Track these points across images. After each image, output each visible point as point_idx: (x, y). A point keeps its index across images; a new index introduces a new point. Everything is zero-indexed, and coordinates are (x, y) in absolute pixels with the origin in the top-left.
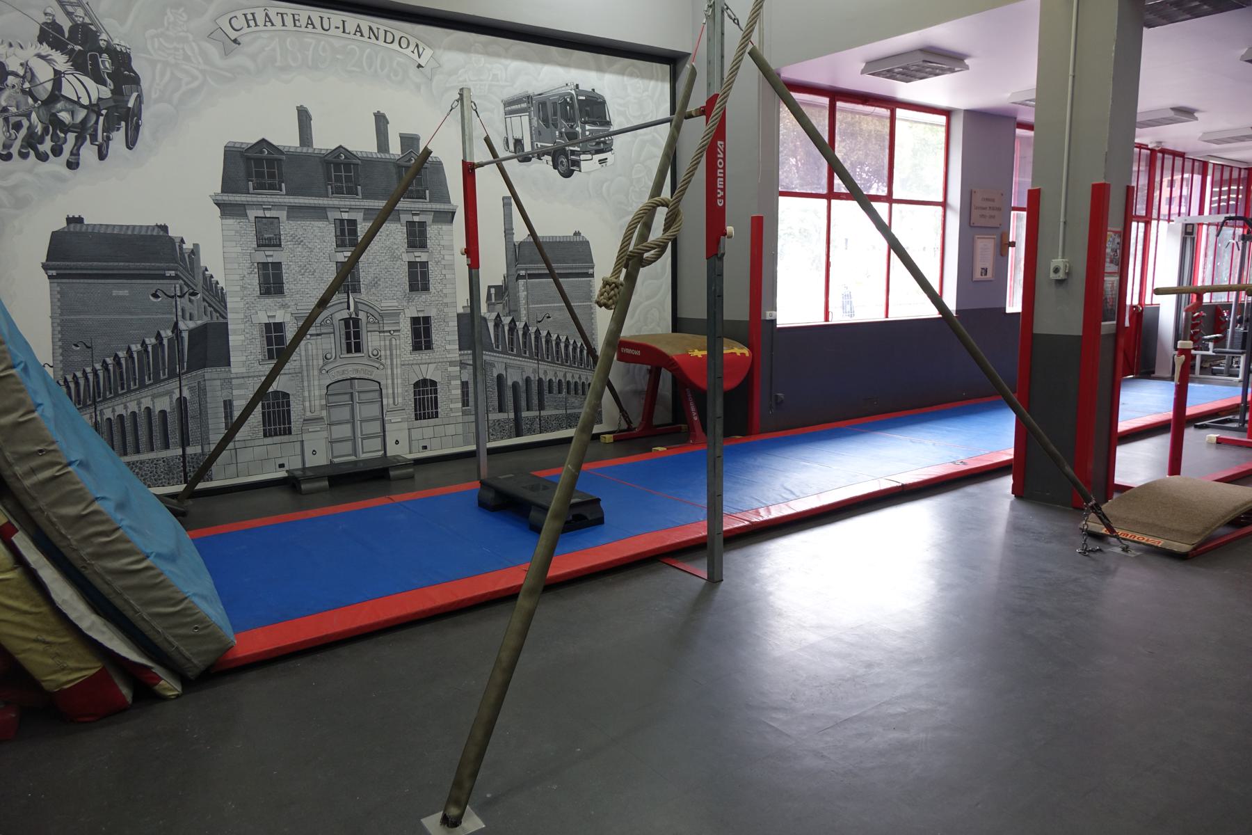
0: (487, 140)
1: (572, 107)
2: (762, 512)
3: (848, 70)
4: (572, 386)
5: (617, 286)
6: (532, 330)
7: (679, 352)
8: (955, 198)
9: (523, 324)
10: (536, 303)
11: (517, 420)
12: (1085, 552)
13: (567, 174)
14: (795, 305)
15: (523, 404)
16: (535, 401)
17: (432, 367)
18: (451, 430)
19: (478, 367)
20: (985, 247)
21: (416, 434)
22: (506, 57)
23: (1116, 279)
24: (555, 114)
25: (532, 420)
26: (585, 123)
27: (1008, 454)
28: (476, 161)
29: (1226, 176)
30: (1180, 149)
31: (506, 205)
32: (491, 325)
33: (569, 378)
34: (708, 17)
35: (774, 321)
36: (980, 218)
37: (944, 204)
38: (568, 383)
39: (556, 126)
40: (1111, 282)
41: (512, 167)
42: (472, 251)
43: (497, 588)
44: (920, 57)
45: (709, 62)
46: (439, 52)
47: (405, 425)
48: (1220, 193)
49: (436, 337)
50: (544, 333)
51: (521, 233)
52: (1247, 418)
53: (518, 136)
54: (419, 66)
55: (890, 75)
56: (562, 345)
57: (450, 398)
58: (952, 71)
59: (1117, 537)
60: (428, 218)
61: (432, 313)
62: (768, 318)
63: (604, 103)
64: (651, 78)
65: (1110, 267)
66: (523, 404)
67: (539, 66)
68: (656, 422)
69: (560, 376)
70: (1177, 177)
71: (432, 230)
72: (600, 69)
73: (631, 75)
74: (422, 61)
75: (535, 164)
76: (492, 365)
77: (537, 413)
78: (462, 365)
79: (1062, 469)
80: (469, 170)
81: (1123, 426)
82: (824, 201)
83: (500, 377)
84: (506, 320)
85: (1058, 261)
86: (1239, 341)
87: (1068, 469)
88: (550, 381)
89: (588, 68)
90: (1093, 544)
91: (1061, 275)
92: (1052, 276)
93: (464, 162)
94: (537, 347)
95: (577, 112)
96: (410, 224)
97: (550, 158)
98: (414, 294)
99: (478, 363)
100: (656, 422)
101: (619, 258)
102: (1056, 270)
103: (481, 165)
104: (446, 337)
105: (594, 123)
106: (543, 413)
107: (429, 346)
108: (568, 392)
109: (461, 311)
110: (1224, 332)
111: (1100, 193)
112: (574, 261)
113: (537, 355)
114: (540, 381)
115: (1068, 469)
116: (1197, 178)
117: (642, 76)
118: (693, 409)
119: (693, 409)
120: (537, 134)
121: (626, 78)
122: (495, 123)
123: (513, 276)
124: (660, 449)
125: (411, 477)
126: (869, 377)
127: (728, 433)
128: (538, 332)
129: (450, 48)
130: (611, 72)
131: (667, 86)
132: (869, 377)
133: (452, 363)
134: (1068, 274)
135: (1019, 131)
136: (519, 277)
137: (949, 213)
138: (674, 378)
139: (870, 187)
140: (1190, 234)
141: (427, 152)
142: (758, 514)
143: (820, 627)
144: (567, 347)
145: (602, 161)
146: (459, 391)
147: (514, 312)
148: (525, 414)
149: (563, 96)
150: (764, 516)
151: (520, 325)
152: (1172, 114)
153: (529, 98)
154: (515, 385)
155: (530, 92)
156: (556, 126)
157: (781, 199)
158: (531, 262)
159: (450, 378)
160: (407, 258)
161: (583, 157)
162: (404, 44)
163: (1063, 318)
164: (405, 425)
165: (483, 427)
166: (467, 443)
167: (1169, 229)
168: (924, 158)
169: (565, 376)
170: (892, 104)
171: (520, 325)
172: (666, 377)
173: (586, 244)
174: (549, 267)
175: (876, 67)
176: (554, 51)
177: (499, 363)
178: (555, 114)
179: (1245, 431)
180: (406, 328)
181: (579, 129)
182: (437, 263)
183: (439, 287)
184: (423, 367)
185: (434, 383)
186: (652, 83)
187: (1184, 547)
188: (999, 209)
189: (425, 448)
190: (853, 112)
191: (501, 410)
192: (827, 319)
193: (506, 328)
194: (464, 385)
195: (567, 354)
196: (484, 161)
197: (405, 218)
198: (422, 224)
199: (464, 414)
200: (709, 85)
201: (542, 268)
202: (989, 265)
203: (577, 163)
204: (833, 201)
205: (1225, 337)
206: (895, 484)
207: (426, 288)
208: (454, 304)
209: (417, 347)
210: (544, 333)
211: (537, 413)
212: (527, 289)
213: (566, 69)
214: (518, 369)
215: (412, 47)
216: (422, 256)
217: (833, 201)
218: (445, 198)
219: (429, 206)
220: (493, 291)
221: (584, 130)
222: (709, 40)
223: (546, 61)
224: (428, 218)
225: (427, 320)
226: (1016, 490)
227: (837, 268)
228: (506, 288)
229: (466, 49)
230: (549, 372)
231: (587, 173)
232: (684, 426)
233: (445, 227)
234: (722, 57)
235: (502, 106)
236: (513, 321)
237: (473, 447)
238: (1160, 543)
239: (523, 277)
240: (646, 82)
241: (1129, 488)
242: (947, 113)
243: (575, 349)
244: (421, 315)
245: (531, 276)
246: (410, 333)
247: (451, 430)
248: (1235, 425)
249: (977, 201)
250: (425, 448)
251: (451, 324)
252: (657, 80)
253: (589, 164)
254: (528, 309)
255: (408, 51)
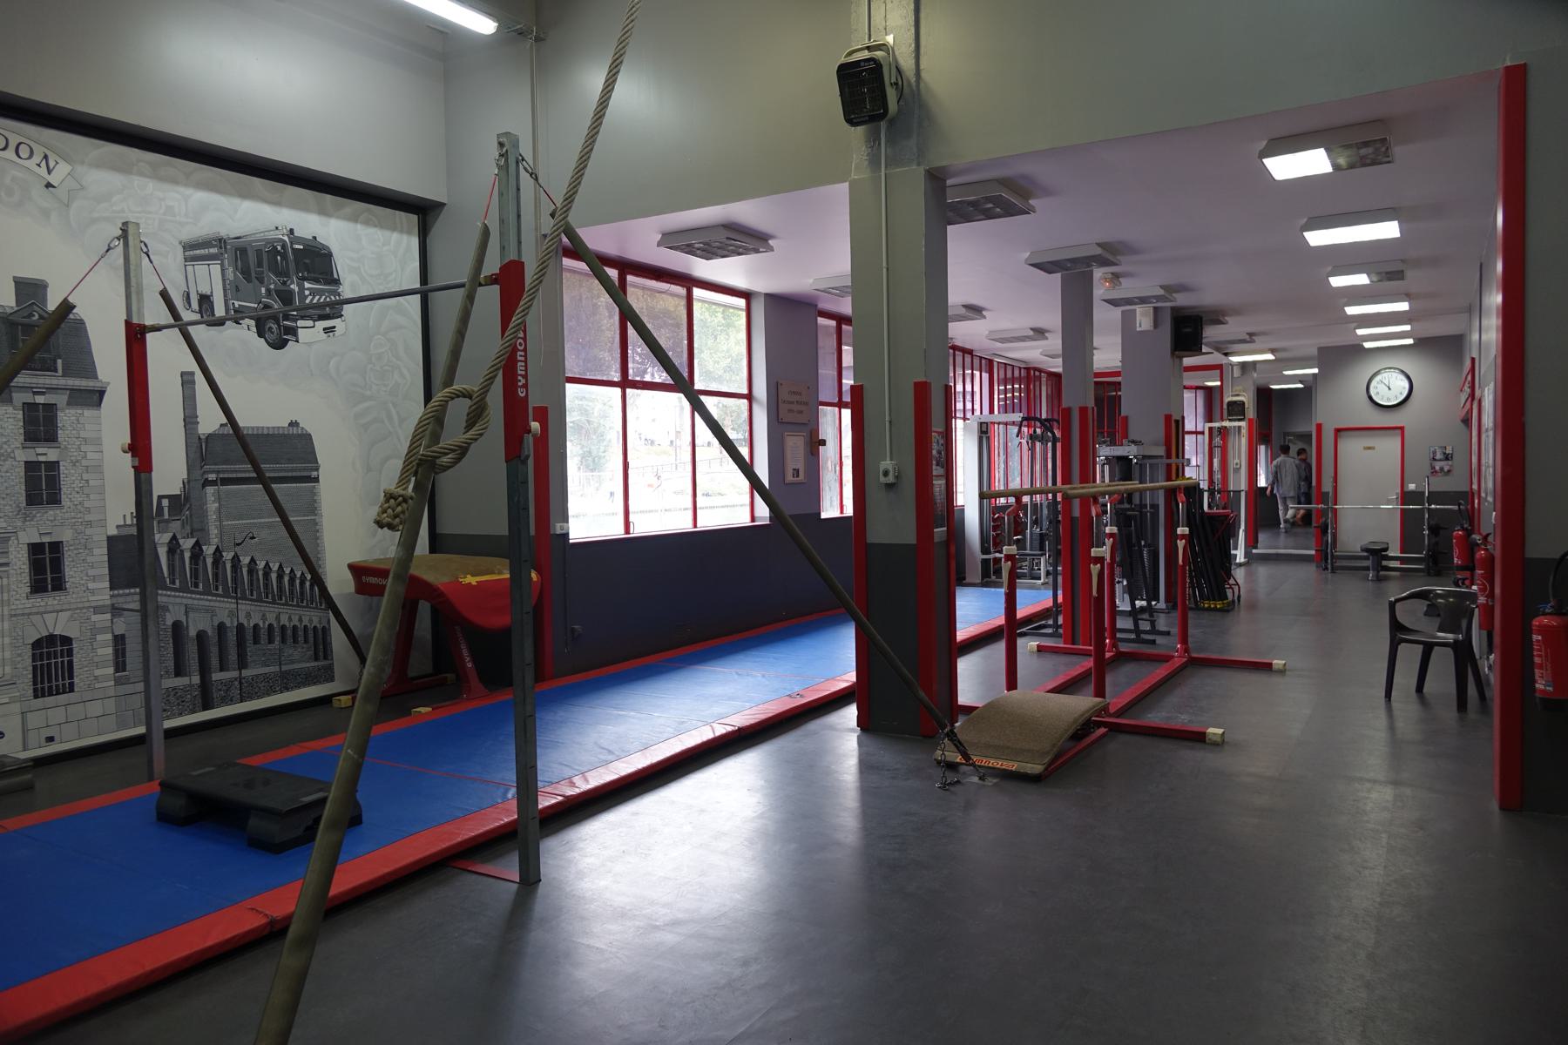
0: (164, 295)
1: (284, 256)
2: (577, 780)
3: (641, 239)
4: (289, 632)
5: (405, 500)
6: (228, 556)
7: (445, 579)
8: (761, 390)
9: (212, 549)
10: (235, 520)
11: (205, 686)
12: (945, 786)
13: (279, 345)
14: (590, 515)
15: (215, 661)
16: (233, 656)
17: (64, 616)
18: (95, 709)
19: (148, 612)
20: (795, 444)
21: (34, 720)
22: (186, 185)
23: (943, 482)
24: (260, 264)
25: (228, 684)
26: (304, 279)
27: (848, 676)
28: (148, 322)
29: (1009, 375)
30: (968, 346)
31: (187, 380)
32: (162, 552)
33: (284, 620)
34: (500, 167)
35: (566, 535)
36: (792, 414)
37: (749, 397)
38: (283, 628)
39: (261, 281)
40: (939, 484)
41: (199, 333)
42: (140, 446)
43: (210, 943)
44: (722, 235)
45: (502, 221)
46: (80, 169)
47: (16, 707)
48: (1006, 391)
49: (71, 571)
50: (245, 560)
51: (210, 420)
52: (1060, 621)
53: (205, 290)
54: (49, 185)
55: (690, 250)
56: (274, 576)
57: (94, 662)
58: (757, 251)
59: (973, 764)
60: (60, 399)
61: (66, 536)
62: (559, 532)
63: (330, 255)
64: (393, 229)
65: (937, 470)
66: (215, 661)
67: (236, 201)
68: (411, 673)
69: (271, 619)
70: (977, 373)
71: (67, 418)
72: (323, 212)
73: (367, 223)
74: (53, 179)
75: (230, 329)
76: (166, 609)
77: (235, 674)
78: (116, 611)
79: (904, 696)
80: (136, 336)
81: (961, 635)
82: (618, 391)
83: (177, 626)
84: (187, 544)
85: (887, 464)
86: (1037, 543)
87: (922, 694)
88: (256, 626)
89: (306, 209)
90: (951, 777)
91: (891, 479)
92: (882, 479)
93: (128, 323)
94: (235, 580)
95: (292, 266)
96: (29, 408)
97: (253, 323)
98: (34, 510)
99: (150, 607)
100: (411, 673)
101: (407, 463)
102: (886, 474)
103: (157, 329)
104: (88, 574)
105: (316, 281)
106: (245, 673)
107: (59, 585)
108: (283, 640)
109: (113, 531)
110: (1023, 532)
111: (922, 390)
112: (290, 461)
113: (235, 591)
114: (240, 627)
115: (922, 694)
116: (986, 376)
117: (381, 225)
118: (465, 653)
119: (465, 653)
120: (232, 290)
121: (359, 226)
122: (168, 269)
123: (197, 481)
124: (423, 710)
125: (29, 787)
126: (683, 601)
127: (539, 677)
128: (236, 560)
129: (100, 165)
130: (338, 217)
131: (415, 241)
132: (683, 601)
133: (98, 610)
134: (897, 477)
135: (821, 320)
136: (207, 483)
137: (755, 407)
138: (435, 612)
139: (645, 372)
140: (984, 431)
141: (66, 307)
142: (573, 784)
143: (676, 923)
144: (280, 577)
145: (328, 330)
146: (110, 650)
147: (199, 532)
148: (217, 676)
149: (271, 242)
150: (582, 786)
151: (209, 550)
152: (963, 311)
153: (221, 242)
154: (201, 636)
155: (224, 233)
156: (261, 281)
157: (568, 385)
158: (226, 462)
159: (95, 631)
160: (23, 456)
161: (300, 323)
162: (24, 152)
163: (895, 527)
164: (16, 707)
165: (156, 703)
166: (122, 725)
167: (965, 428)
168: (725, 349)
169: (278, 618)
170: (689, 282)
171: (209, 550)
172: (424, 609)
173: (307, 438)
174: (257, 468)
175: (672, 239)
176: (257, 182)
177: (174, 605)
178: (260, 264)
179: (1060, 636)
180: (19, 559)
181: (294, 287)
182: (74, 464)
183: (78, 498)
184: (49, 618)
185: (67, 640)
186: (395, 236)
187: (1035, 768)
188: (806, 404)
189: (50, 739)
190: (644, 288)
191: (179, 672)
192: (627, 531)
193: (187, 555)
194: (119, 641)
195: (302, 593)
196: (163, 322)
197: (20, 398)
198: (51, 408)
199: (118, 682)
200: (503, 248)
201: (246, 470)
202: (801, 466)
203: (293, 331)
204: (628, 391)
205: (1024, 539)
206: (730, 729)
207: (55, 500)
208: (103, 523)
209: (38, 587)
210: (245, 560)
211: (235, 674)
212: (219, 499)
213: (277, 209)
214: (202, 612)
215: (37, 158)
216: (51, 455)
217: (628, 391)
218: (87, 368)
219: (62, 382)
220: (165, 502)
221: (302, 289)
222: (501, 194)
223: (245, 195)
224: (60, 399)
225: (56, 547)
226: (861, 722)
227: (647, 467)
228: (187, 499)
229: (125, 169)
230: (253, 614)
231: (309, 344)
232: (450, 676)
233: (88, 413)
234: (519, 216)
235: (180, 249)
236: (197, 544)
237: (142, 730)
238: (1013, 766)
239: (213, 483)
240: (387, 233)
241: (975, 708)
242: (746, 295)
243: (292, 580)
244: (46, 539)
245: (225, 482)
246: (26, 568)
247: (95, 709)
248: (1050, 631)
249: (784, 395)
250: (50, 739)
251: (96, 551)
252: (401, 232)
253: (310, 332)
254: (221, 528)
255: (31, 164)
